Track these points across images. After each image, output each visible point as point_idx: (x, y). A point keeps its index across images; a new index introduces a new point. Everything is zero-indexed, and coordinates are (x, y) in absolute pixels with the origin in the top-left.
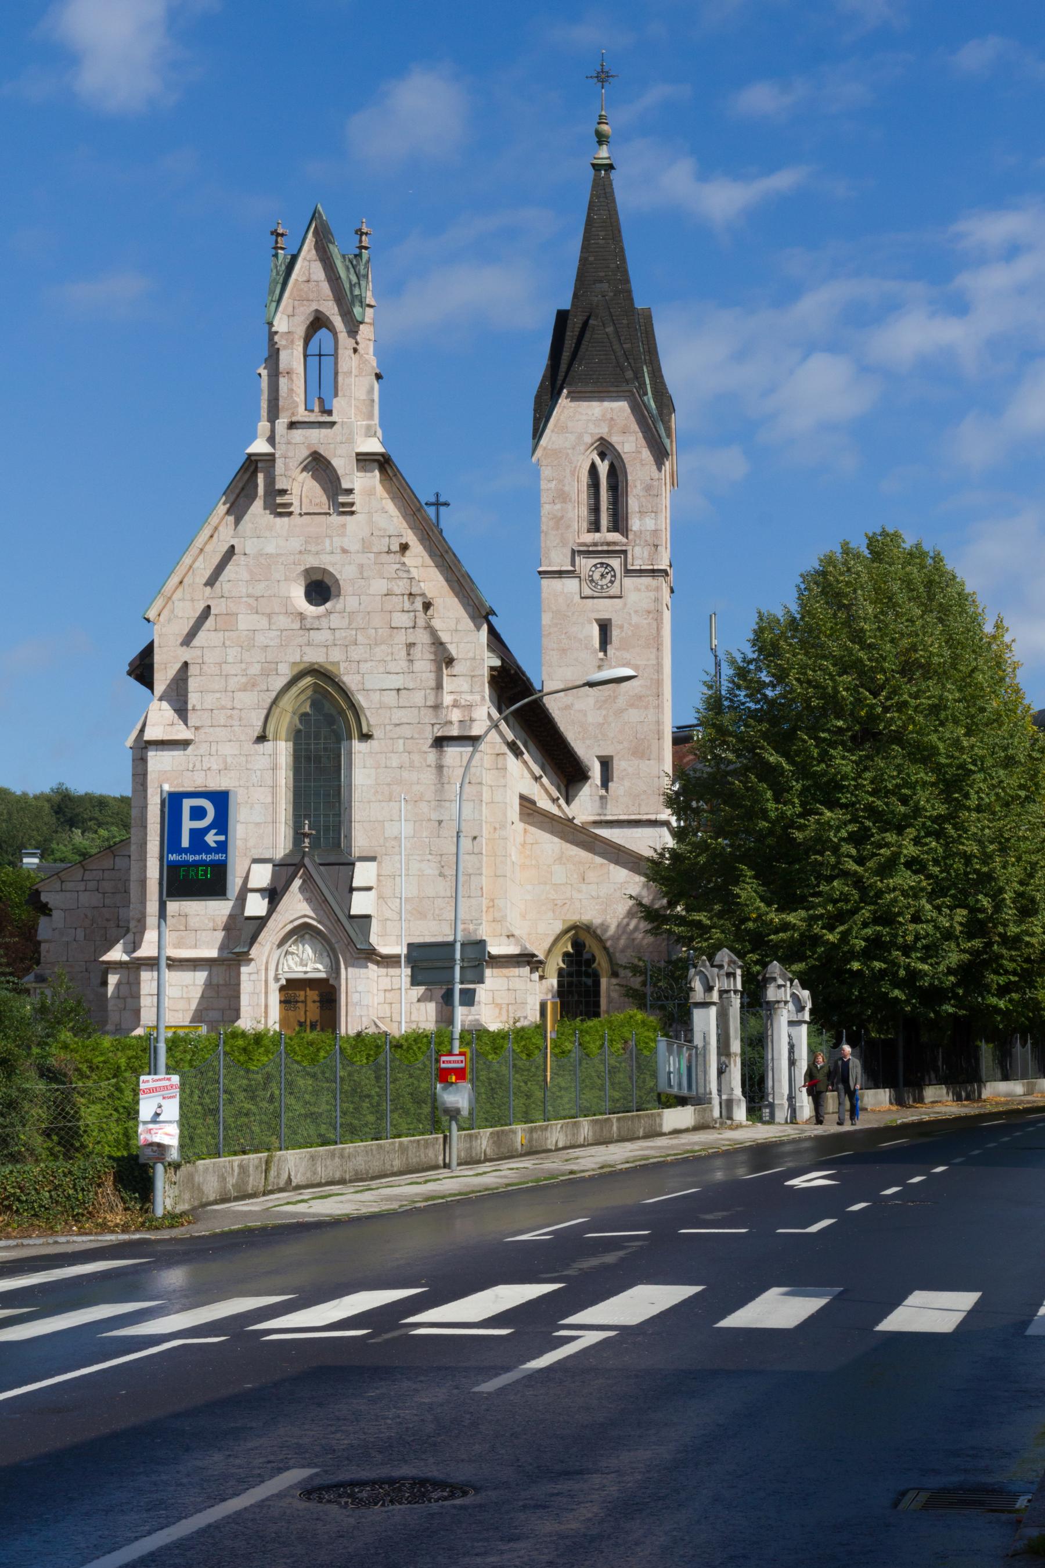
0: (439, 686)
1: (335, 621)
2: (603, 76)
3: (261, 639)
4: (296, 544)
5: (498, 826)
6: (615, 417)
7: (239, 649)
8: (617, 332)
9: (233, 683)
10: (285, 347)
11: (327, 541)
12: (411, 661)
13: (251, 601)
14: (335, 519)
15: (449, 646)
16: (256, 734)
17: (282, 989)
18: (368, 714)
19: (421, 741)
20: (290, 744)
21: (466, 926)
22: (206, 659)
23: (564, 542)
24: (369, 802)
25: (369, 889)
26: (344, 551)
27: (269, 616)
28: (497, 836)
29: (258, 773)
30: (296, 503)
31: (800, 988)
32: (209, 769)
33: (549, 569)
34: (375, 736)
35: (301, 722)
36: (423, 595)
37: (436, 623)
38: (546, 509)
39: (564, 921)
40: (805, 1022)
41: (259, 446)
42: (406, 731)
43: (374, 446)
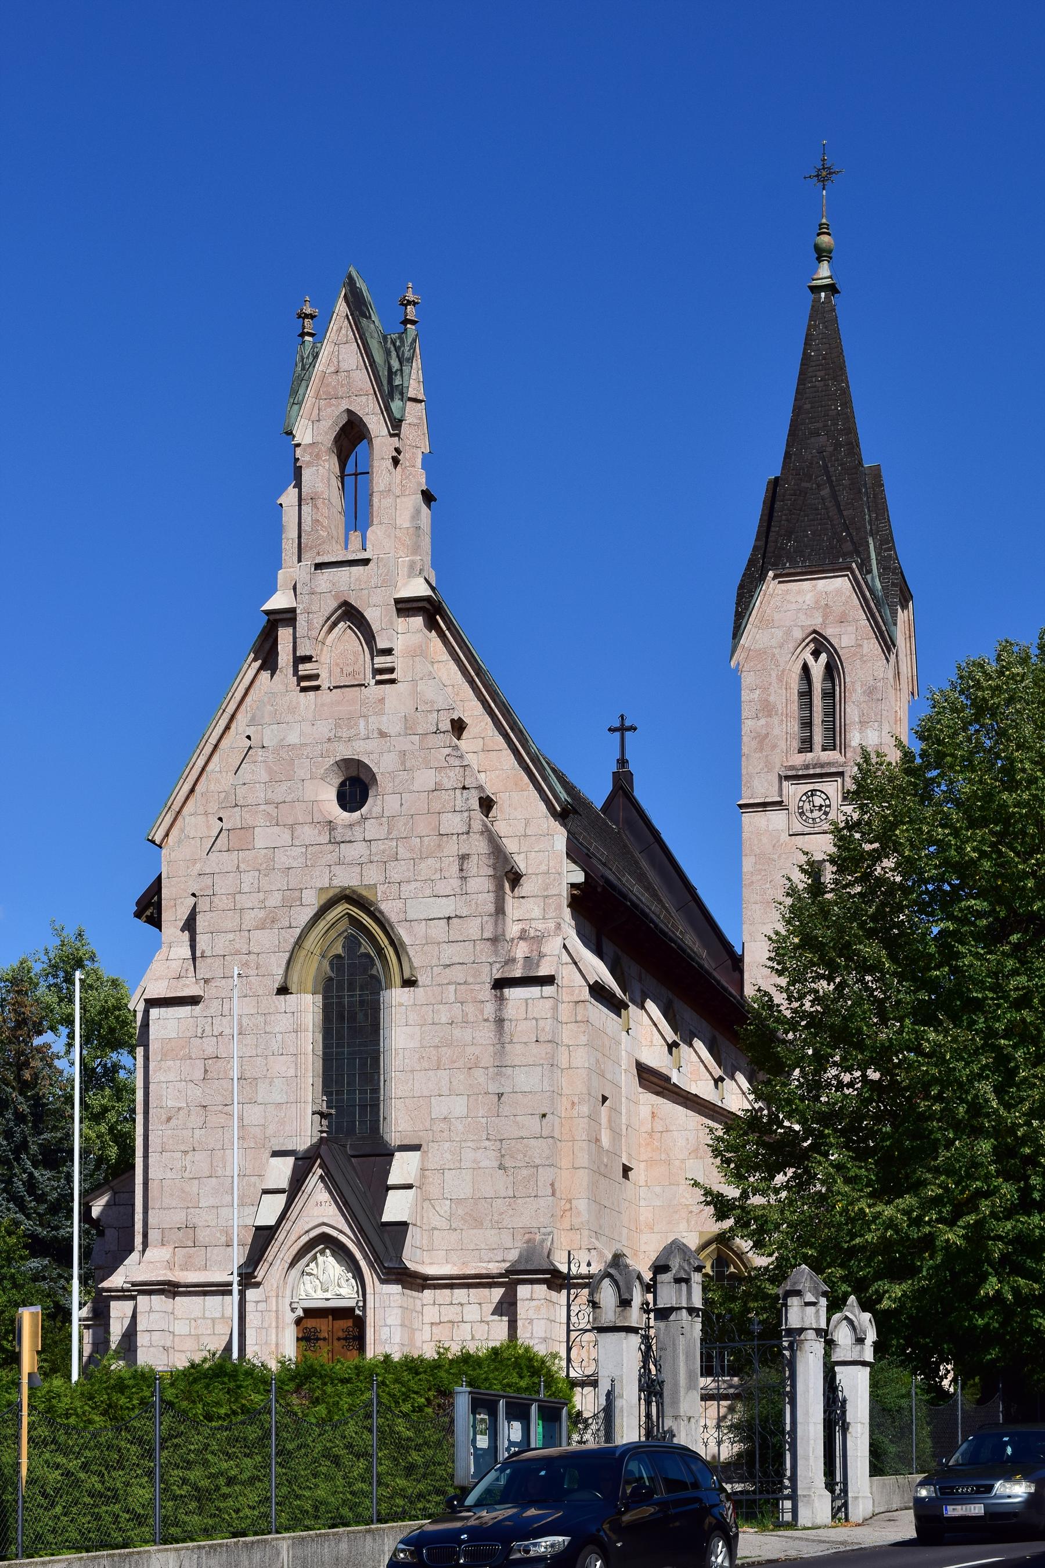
0: (500, 910)
1: (372, 829)
2: (824, 173)
3: (282, 859)
4: (324, 729)
5: (576, 1101)
6: (831, 604)
7: (257, 874)
8: (834, 495)
9: (251, 918)
10: (309, 464)
11: (362, 723)
12: (464, 878)
13: (270, 809)
14: (375, 691)
15: (516, 857)
16: (276, 985)
17: (298, 1322)
18: (411, 953)
19: (477, 987)
20: (319, 998)
21: (531, 1236)
22: (217, 889)
23: (769, 766)
24: (412, 1071)
25: (409, 1187)
26: (383, 734)
27: (292, 827)
28: (575, 1113)
29: (279, 1037)
30: (324, 674)
31: (857, 1310)
32: (221, 1034)
33: (751, 801)
34: (420, 983)
35: (332, 969)
36: (480, 788)
37: (501, 828)
38: (748, 726)
39: (701, 1233)
40: (864, 1364)
41: (279, 601)
42: (458, 974)
43: (418, 588)
